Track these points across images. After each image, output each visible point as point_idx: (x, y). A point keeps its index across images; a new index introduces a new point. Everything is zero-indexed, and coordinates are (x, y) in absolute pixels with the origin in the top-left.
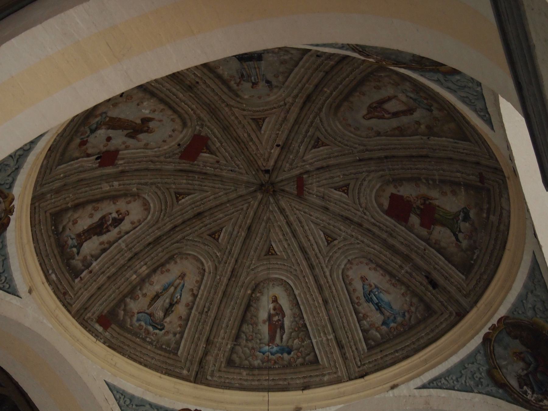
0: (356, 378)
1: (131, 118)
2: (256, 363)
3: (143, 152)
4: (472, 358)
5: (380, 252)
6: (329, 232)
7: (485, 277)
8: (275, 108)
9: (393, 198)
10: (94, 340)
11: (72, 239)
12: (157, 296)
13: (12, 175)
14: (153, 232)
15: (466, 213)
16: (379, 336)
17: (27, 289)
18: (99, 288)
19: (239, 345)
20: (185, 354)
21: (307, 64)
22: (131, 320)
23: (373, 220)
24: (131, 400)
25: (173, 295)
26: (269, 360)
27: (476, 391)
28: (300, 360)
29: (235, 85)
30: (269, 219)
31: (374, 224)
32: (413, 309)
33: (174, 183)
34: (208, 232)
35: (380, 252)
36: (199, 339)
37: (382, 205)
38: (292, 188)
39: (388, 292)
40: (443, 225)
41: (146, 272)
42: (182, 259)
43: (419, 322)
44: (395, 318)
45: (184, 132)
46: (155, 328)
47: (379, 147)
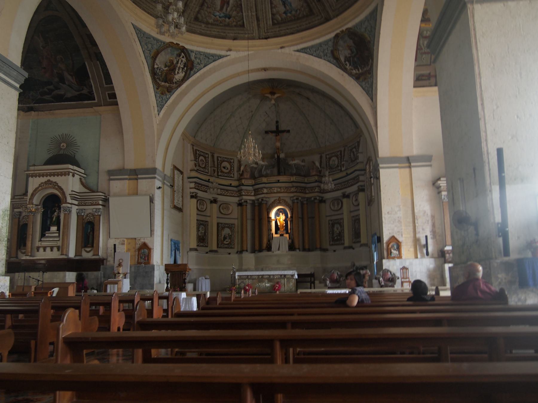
0: (263, 39)
2: (211, 21)
4: (326, 43)
16: (280, 19)
19: (203, 9)
26: (217, 21)
27: (323, 58)
28: (234, 23)
32: (303, 9)
44: (291, 11)
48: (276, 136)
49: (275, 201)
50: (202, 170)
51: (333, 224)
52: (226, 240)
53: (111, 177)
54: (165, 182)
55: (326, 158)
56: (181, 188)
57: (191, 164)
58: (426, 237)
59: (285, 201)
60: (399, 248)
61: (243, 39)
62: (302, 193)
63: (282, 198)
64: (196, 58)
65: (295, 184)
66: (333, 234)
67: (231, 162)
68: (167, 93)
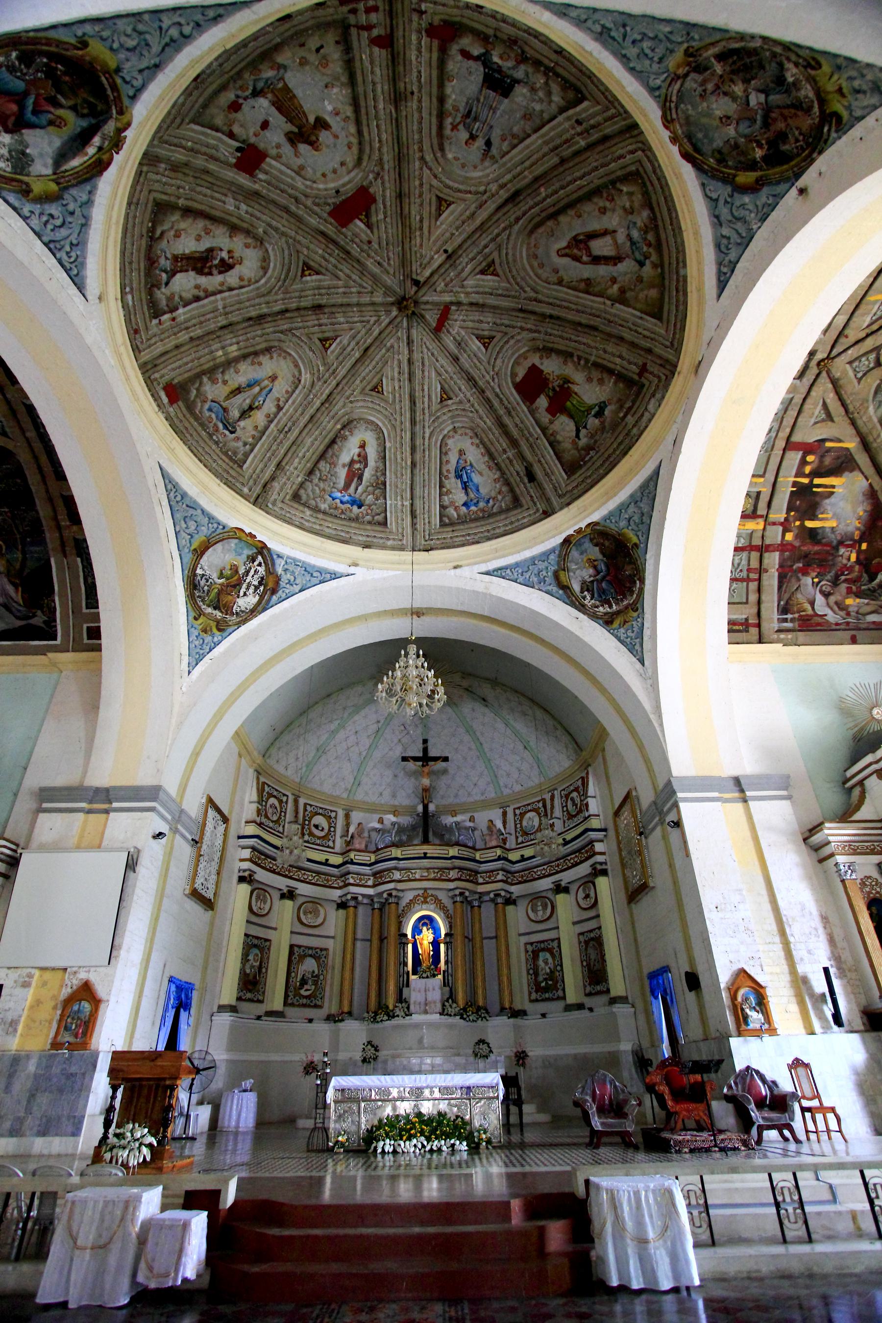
1: (306, 107)
2: (323, 506)
3: (292, 178)
4: (545, 556)
5: (490, 429)
6: (446, 386)
7: (589, 481)
8: (470, 192)
9: (534, 371)
10: (157, 409)
11: (167, 258)
12: (238, 390)
13: (146, 72)
14: (260, 304)
15: (602, 406)
17: (97, 293)
18: (177, 347)
20: (251, 471)
21: (552, 134)
22: (202, 406)
23: (498, 390)
24: (182, 498)
25: (255, 397)
26: (336, 508)
28: (368, 518)
29: (449, 127)
30: (392, 346)
31: (497, 395)
32: (500, 497)
33: (308, 248)
34: (320, 336)
35: (490, 429)
36: (270, 459)
37: (516, 375)
38: (432, 317)
39: (481, 474)
40: (571, 416)
41: (236, 354)
42: (280, 355)
43: (501, 512)
45: (353, 174)
46: (226, 427)
47: (551, 300)
48: (423, 766)
49: (415, 897)
50: (271, 825)
51: (535, 952)
52: (306, 987)
53: (45, 805)
54: (179, 827)
55: (515, 815)
56: (219, 854)
57: (250, 810)
58: (826, 970)
59: (436, 898)
60: (762, 1003)
61: (383, 547)
62: (471, 881)
63: (430, 892)
64: (286, 570)
65: (458, 863)
66: (536, 974)
67: (330, 817)
68: (215, 630)
